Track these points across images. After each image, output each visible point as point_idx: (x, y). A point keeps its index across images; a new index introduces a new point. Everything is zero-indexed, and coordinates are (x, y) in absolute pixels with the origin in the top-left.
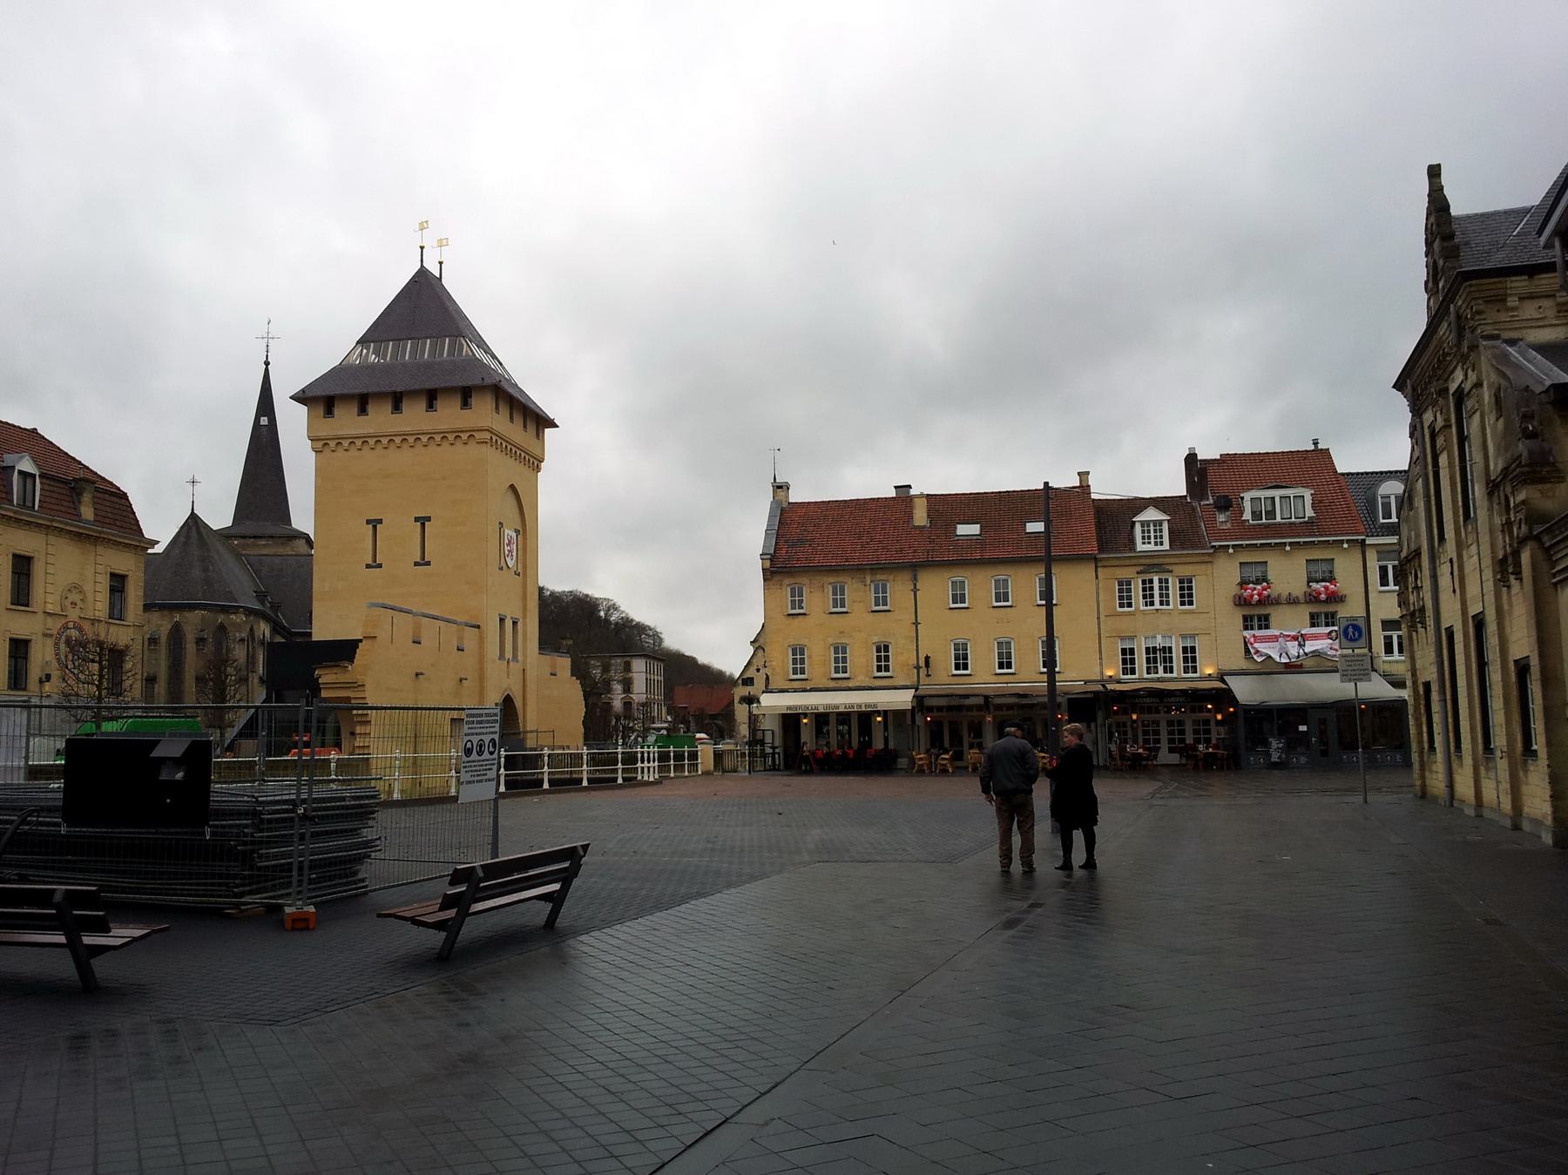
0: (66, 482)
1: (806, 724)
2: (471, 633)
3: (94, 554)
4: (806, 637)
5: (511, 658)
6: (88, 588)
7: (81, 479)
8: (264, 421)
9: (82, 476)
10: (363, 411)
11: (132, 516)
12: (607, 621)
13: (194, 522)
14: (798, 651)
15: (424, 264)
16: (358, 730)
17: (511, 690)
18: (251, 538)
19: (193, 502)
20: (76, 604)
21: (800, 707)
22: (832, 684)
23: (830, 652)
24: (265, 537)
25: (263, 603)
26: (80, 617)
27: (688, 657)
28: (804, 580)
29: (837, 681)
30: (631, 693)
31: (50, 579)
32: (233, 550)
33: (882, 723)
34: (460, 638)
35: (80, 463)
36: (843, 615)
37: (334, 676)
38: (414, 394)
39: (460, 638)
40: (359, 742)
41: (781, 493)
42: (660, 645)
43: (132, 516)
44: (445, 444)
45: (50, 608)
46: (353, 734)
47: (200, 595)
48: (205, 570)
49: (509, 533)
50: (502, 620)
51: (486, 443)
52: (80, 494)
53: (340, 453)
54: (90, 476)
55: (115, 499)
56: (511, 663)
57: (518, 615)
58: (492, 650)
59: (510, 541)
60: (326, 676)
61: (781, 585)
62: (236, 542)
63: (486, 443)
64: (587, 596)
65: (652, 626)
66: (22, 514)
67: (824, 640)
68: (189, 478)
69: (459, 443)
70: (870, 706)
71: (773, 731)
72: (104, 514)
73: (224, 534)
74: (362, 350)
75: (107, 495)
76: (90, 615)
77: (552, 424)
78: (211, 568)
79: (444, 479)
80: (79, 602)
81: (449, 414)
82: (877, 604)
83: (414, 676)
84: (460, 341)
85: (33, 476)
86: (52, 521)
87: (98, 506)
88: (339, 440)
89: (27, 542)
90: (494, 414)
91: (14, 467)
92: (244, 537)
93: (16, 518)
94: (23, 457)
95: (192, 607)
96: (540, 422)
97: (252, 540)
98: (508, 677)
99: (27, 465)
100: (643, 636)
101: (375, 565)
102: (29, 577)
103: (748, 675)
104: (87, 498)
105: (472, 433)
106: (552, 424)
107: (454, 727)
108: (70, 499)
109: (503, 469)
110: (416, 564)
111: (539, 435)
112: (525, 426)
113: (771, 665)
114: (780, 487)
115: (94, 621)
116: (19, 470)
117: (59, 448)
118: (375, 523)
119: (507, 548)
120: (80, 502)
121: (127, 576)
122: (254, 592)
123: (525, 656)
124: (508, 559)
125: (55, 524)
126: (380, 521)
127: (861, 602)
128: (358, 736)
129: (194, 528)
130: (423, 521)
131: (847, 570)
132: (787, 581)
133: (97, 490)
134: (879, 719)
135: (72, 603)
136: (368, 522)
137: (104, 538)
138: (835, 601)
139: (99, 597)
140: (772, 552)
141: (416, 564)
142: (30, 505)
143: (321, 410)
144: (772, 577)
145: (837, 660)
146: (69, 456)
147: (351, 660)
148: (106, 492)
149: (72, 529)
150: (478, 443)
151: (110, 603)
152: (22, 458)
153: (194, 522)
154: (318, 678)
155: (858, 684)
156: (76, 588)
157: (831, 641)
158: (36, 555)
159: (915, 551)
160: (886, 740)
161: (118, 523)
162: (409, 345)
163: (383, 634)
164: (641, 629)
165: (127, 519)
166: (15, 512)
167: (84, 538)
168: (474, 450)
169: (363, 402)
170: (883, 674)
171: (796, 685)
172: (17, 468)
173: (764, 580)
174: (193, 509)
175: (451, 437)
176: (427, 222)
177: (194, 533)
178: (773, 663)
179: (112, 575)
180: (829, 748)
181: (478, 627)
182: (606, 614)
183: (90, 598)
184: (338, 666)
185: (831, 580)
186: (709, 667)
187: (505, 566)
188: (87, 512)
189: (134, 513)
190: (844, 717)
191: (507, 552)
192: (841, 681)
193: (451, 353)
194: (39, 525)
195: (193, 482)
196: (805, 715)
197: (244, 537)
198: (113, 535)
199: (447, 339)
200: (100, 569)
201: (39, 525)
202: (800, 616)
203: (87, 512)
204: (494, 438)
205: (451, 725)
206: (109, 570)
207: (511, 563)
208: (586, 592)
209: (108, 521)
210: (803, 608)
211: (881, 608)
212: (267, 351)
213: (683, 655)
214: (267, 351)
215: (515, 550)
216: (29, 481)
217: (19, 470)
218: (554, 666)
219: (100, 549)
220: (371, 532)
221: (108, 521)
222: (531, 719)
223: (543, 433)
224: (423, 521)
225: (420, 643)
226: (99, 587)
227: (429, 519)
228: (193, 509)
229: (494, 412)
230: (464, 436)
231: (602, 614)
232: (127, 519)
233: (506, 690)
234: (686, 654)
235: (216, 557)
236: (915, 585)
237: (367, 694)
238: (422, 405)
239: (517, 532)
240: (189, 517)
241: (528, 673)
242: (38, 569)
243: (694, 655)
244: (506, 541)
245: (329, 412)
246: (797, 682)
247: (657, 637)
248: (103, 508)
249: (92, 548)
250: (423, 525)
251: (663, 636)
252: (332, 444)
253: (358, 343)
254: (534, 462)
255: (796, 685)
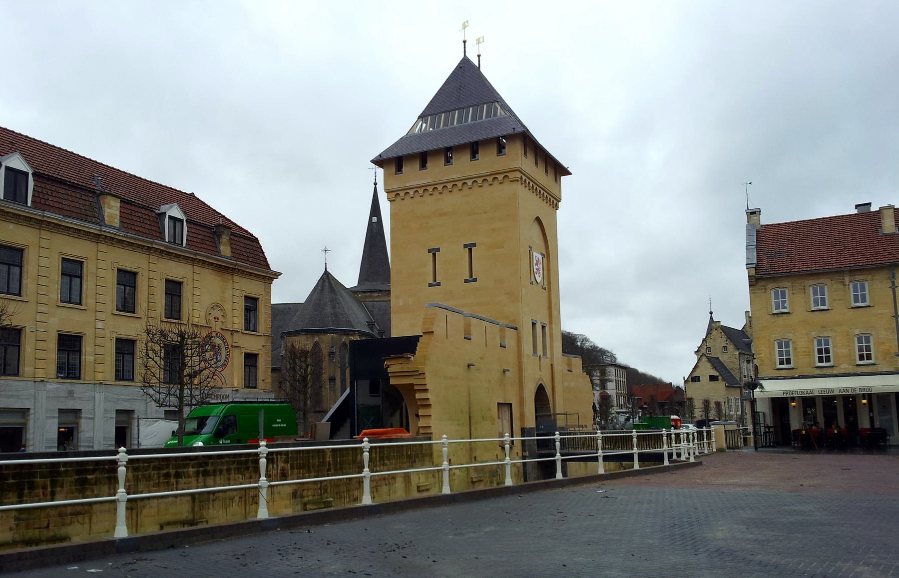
0: (210, 228)
1: (794, 406)
2: (510, 333)
3: (231, 282)
4: (791, 333)
5: (542, 355)
6: (228, 307)
7: (220, 225)
8: (375, 219)
9: (221, 223)
10: (423, 165)
11: (261, 255)
12: (582, 348)
13: (327, 278)
14: (783, 344)
15: (466, 54)
16: (421, 412)
17: (542, 380)
18: (368, 292)
19: (326, 264)
20: (218, 319)
21: (796, 392)
22: (817, 372)
23: (813, 345)
24: (377, 291)
25: (372, 330)
26: (222, 329)
27: (632, 369)
28: (787, 284)
29: (822, 369)
30: (606, 389)
31: (196, 299)
32: (359, 302)
33: (867, 404)
34: (502, 337)
35: (220, 214)
36: (824, 312)
37: (400, 366)
38: (460, 148)
39: (502, 337)
40: (422, 423)
41: (754, 217)
42: (615, 362)
43: (260, 250)
44: (486, 185)
45: (196, 321)
46: (417, 416)
47: (331, 323)
48: (334, 307)
49: (537, 256)
50: (534, 324)
51: (518, 181)
52: (219, 236)
53: (408, 200)
54: (230, 225)
55: (248, 242)
56: (542, 359)
57: (546, 321)
58: (527, 348)
59: (537, 262)
60: (394, 367)
61: (765, 289)
62: (360, 295)
63: (518, 181)
64: (569, 333)
65: (610, 350)
66: (171, 248)
67: (807, 334)
68: (323, 248)
69: (496, 183)
70: (864, 389)
71: (764, 413)
72: (239, 252)
73: (353, 291)
74: (422, 125)
75: (242, 239)
76: (229, 327)
77: (566, 172)
78: (337, 305)
79: (485, 212)
80: (220, 317)
81: (488, 161)
82: (856, 301)
83: (467, 367)
84: (495, 105)
85: (182, 221)
86: (196, 254)
87: (235, 247)
88: (406, 190)
89: (177, 270)
90: (524, 158)
91: (165, 213)
92: (364, 292)
93: (167, 252)
94: (174, 205)
95: (326, 332)
96: (560, 170)
97: (369, 293)
98: (540, 371)
99: (175, 211)
100: (604, 357)
101: (435, 284)
102: (180, 298)
103: (695, 374)
104: (225, 238)
105: (506, 174)
106: (566, 172)
107: (500, 410)
108: (212, 240)
109: (529, 203)
110: (466, 281)
111: (557, 180)
112: (546, 172)
113: (760, 358)
114: (753, 213)
115: (233, 332)
116: (169, 216)
117: (209, 207)
118: (434, 252)
119: (535, 267)
120: (219, 243)
121: (258, 299)
122: (367, 322)
123: (552, 354)
124: (537, 276)
125: (199, 257)
126: (438, 250)
127: (840, 300)
128: (421, 417)
129: (327, 280)
130: (470, 247)
131: (831, 272)
132: (770, 286)
133: (233, 234)
134: (864, 401)
135: (215, 318)
136: (429, 251)
137: (239, 270)
138: (816, 301)
139: (236, 313)
140: (756, 262)
141: (466, 281)
142: (180, 243)
143: (393, 169)
144: (757, 282)
145: (820, 351)
146: (211, 208)
147: (413, 351)
148: (241, 236)
149: (214, 262)
150: (511, 181)
151: (246, 319)
152: (171, 207)
153: (327, 278)
154: (387, 368)
155: (842, 371)
156: (217, 306)
157: (814, 334)
158: (185, 280)
159: (890, 254)
160: (872, 420)
161: (251, 259)
162: (457, 113)
163: (439, 329)
164: (603, 352)
165: (257, 257)
166: (165, 247)
167: (223, 269)
168: (508, 188)
169: (423, 158)
170: (865, 362)
171: (784, 373)
172: (168, 214)
173: (750, 286)
174: (326, 268)
175: (490, 179)
176: (467, 22)
177: (327, 284)
178: (761, 356)
179: (246, 297)
180: (818, 427)
181: (516, 329)
182: (581, 344)
183: (229, 315)
184: (403, 357)
185: (811, 282)
186: (646, 375)
187: (534, 282)
188: (225, 250)
189: (263, 253)
190: (829, 401)
191: (535, 271)
192: (825, 369)
193: (488, 115)
194: (187, 258)
195: (326, 251)
196: (793, 399)
197: (364, 292)
198: (246, 267)
199: (485, 106)
200: (237, 293)
201: (187, 258)
202: (785, 315)
203: (225, 250)
204: (524, 178)
205: (498, 407)
206: (244, 294)
207: (539, 279)
208: (568, 331)
209: (242, 257)
210: (786, 308)
211: (860, 304)
212: (375, 177)
213: (629, 368)
214: (375, 177)
215: (541, 270)
216: (178, 225)
217: (169, 216)
218: (569, 364)
219: (236, 278)
220: (431, 259)
221: (242, 257)
222: (560, 404)
223: (560, 179)
224: (470, 247)
225: (470, 339)
226: (236, 306)
227: (474, 245)
228: (326, 268)
229: (523, 156)
230: (500, 177)
231: (579, 344)
232: (257, 257)
233: (539, 380)
234: (631, 367)
235: (341, 299)
236: (893, 283)
237: (427, 381)
238: (467, 156)
239: (543, 255)
240: (323, 274)
241: (555, 366)
242: (187, 291)
243: (636, 368)
244: (535, 262)
245: (399, 169)
246: (784, 371)
247: (612, 357)
248: (238, 248)
249: (230, 277)
250: (470, 250)
251: (616, 356)
252: (402, 194)
253: (419, 117)
254: (554, 201)
255: (784, 373)
